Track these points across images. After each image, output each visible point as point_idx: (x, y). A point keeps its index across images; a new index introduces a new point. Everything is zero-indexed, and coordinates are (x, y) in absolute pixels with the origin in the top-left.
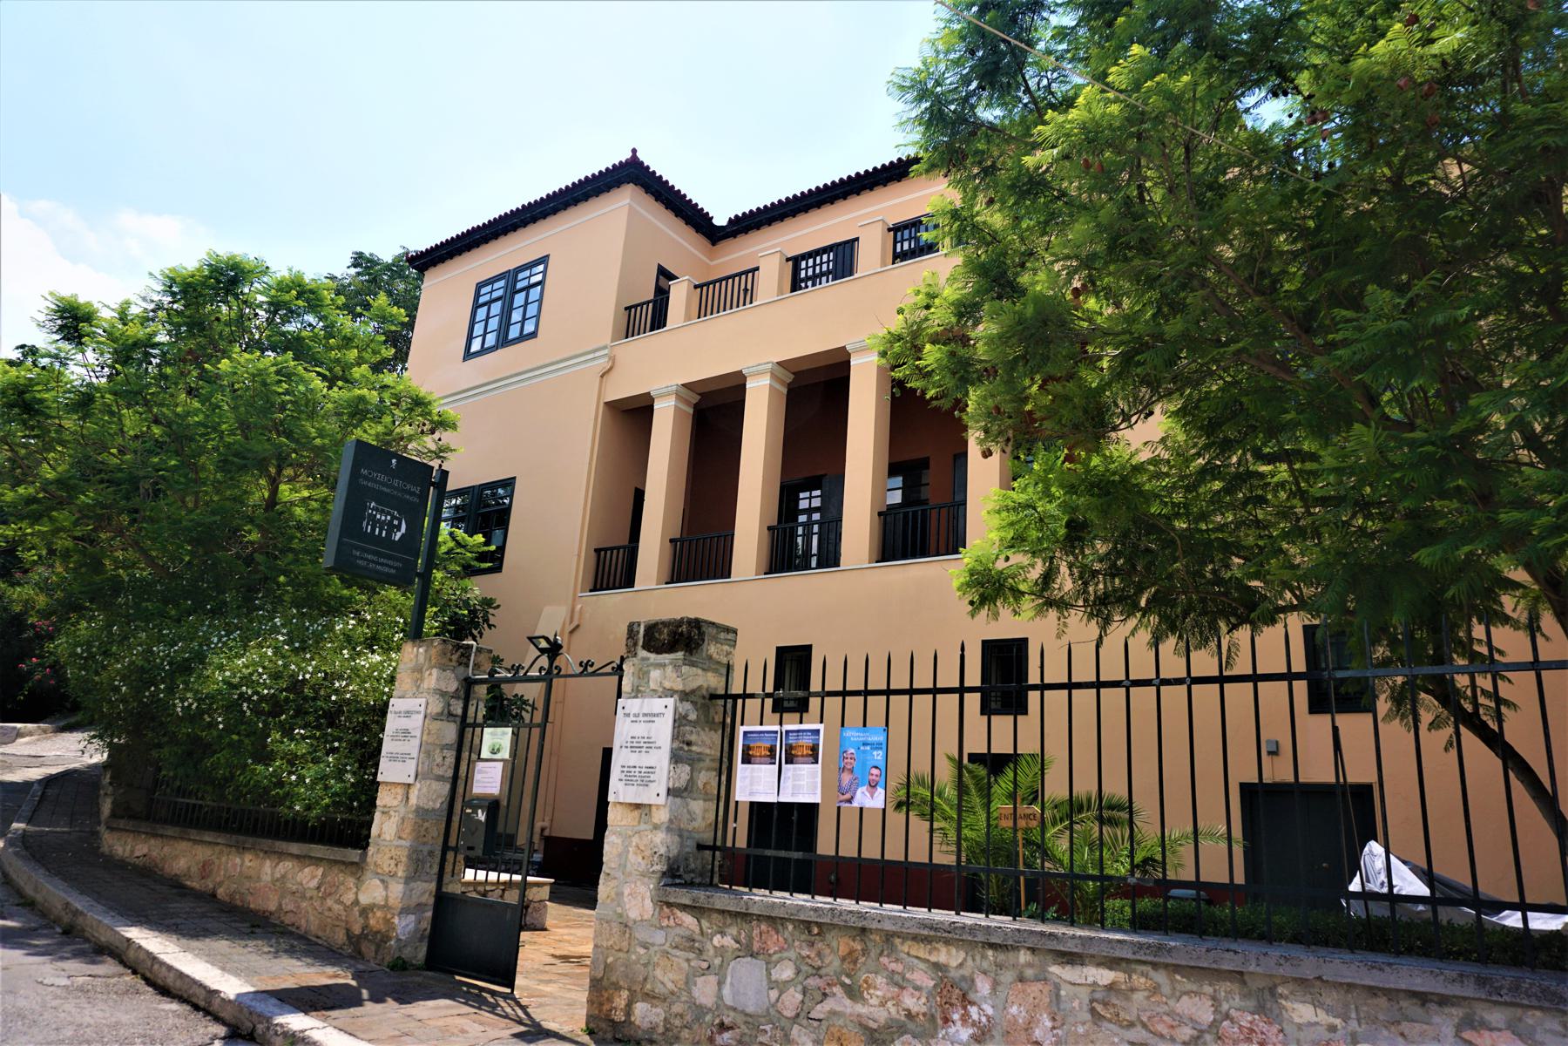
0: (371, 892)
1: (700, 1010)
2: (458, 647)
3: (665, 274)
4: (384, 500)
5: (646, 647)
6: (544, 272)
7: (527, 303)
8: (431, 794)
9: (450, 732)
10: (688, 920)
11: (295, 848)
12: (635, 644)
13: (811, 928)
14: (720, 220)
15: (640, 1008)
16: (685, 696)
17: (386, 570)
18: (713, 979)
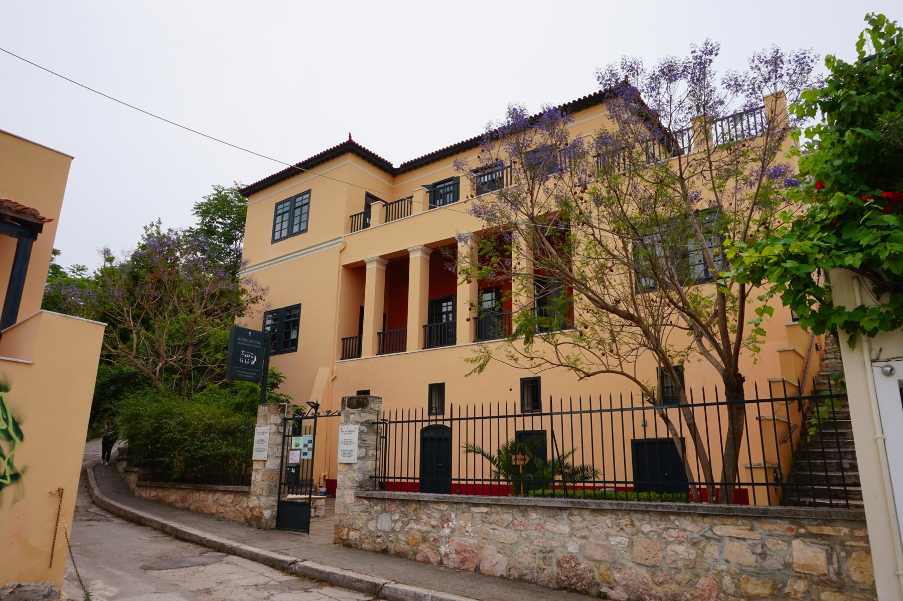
0: (253, 502)
1: (371, 532)
2: (280, 406)
4: (248, 349)
6: (309, 198)
7: (301, 214)
8: (273, 464)
9: (279, 439)
10: (366, 502)
11: (222, 488)
13: (404, 502)
14: (396, 166)
15: (352, 534)
16: (362, 424)
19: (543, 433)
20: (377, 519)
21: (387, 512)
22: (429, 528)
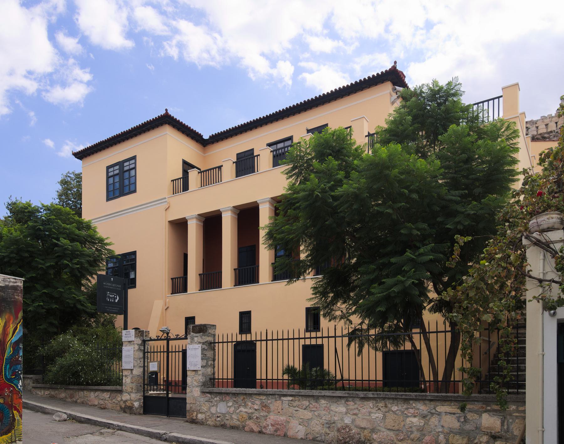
0: (125, 397)
4: (112, 291)
6: (135, 163)
8: (138, 371)
9: (141, 355)
10: (209, 395)
14: (206, 137)
16: (203, 343)
19: (305, 347)
20: (217, 406)
21: (224, 401)
22: (253, 411)
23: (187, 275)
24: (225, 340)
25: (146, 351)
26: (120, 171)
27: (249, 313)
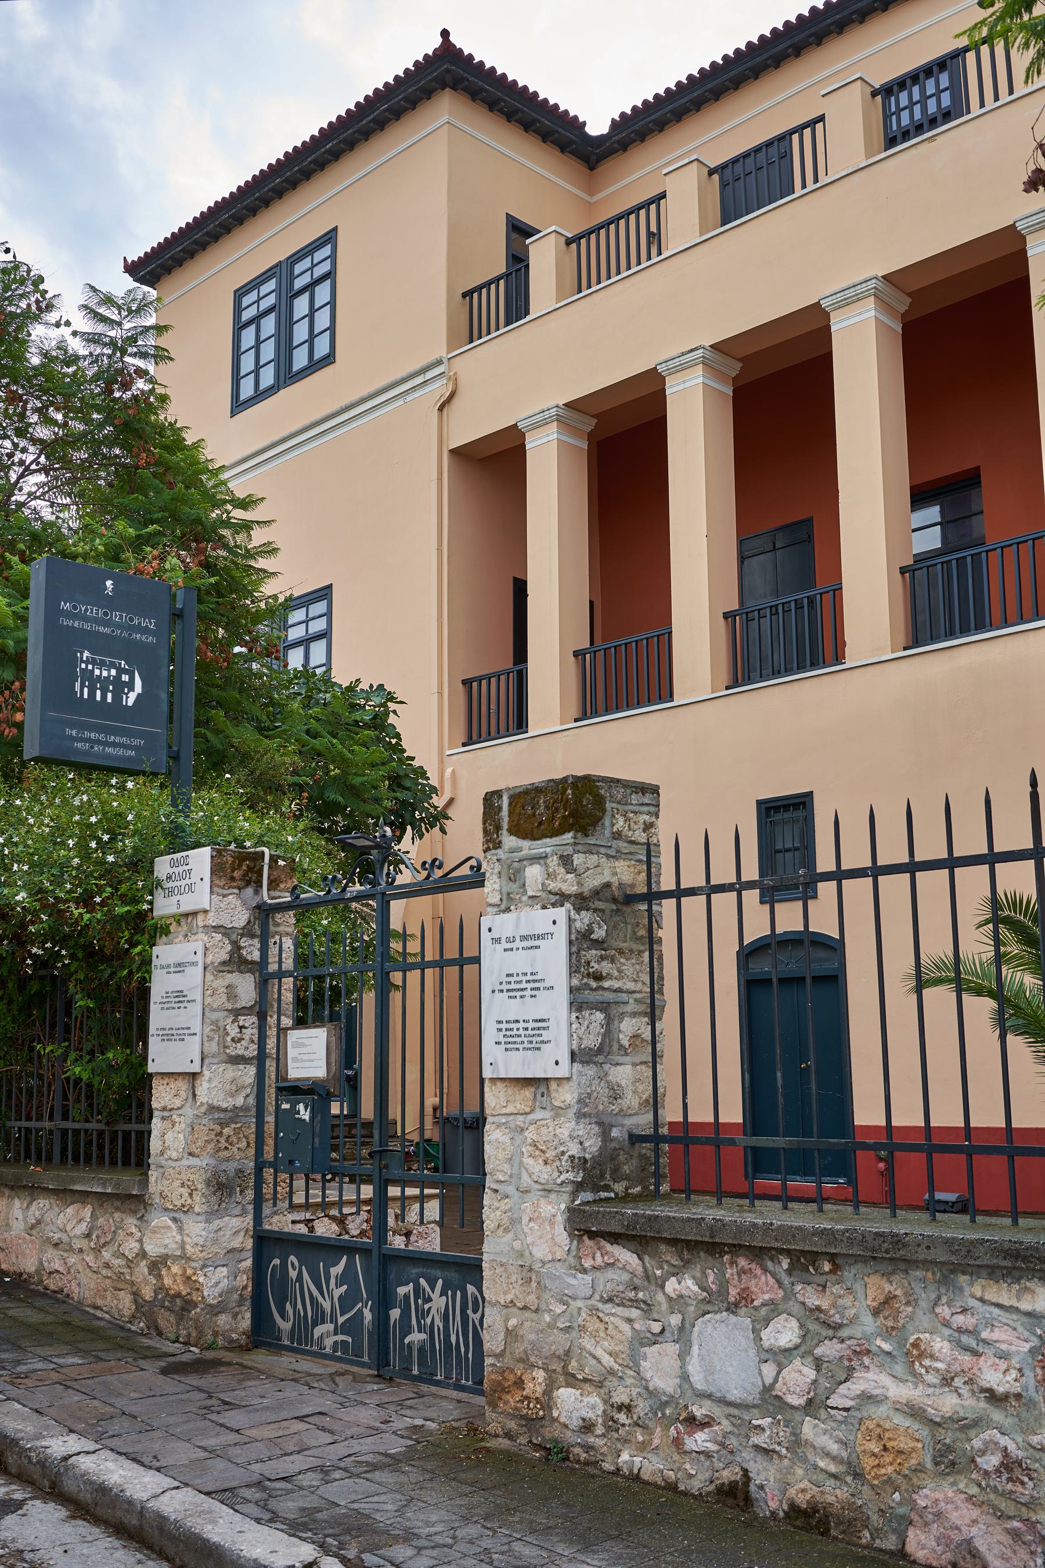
0: (161, 1236)
3: (519, 231)
4: (104, 647)
5: (516, 831)
7: (313, 311)
8: (224, 1086)
10: (625, 1255)
12: (498, 828)
14: (597, 126)
15: (565, 1395)
16: (581, 902)
17: (121, 752)
18: (673, 1349)
20: (683, 1336)
21: (733, 1308)
22: (971, 1405)
23: (525, 661)
24: (893, 852)
25: (273, 967)
26: (279, 298)
27: (799, 805)
